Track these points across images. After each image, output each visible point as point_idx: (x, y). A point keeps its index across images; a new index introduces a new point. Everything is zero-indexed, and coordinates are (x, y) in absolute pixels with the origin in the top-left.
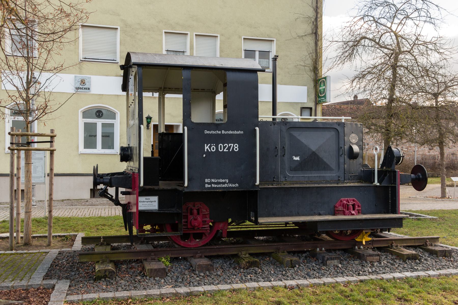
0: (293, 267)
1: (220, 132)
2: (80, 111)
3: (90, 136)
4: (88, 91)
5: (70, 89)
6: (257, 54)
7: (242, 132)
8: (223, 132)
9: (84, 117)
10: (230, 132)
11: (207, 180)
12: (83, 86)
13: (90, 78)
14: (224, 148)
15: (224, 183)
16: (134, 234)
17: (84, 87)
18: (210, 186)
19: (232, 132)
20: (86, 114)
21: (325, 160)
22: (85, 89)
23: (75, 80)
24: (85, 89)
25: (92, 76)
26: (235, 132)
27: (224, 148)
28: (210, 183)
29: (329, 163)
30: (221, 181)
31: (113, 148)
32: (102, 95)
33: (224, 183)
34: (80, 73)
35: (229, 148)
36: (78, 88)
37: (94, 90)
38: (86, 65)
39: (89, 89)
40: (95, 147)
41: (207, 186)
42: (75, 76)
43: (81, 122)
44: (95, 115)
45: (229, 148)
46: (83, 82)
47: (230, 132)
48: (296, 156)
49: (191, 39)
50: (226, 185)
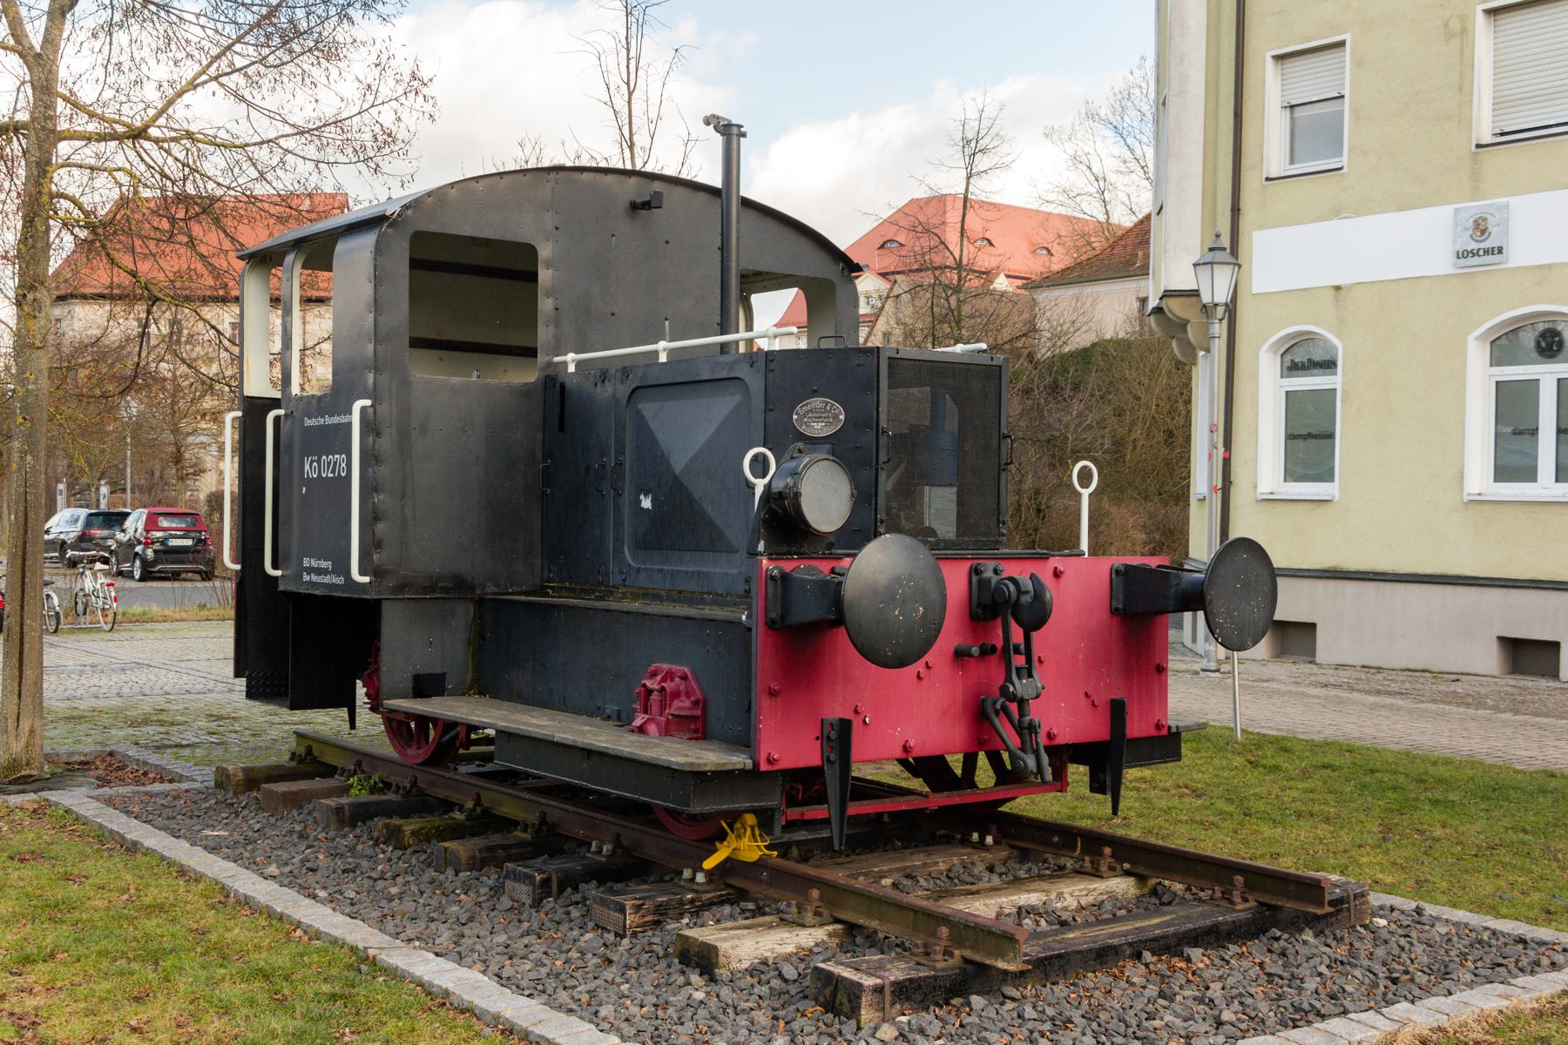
1: (322, 421)
3: (1517, 433)
4: (1496, 258)
5: (1442, 263)
9: (1496, 361)
11: (306, 562)
12: (1481, 245)
13: (1507, 206)
15: (319, 571)
16: (1083, 769)
17: (1483, 245)
19: (322, 421)
20: (1503, 346)
21: (709, 509)
22: (1486, 252)
23: (1456, 226)
24: (1486, 252)
25: (1511, 200)
29: (719, 523)
32: (1550, 266)
34: (1475, 195)
36: (1462, 255)
37: (1521, 253)
38: (1497, 161)
39: (1500, 250)
40: (1529, 474)
41: (306, 578)
42: (1456, 210)
43: (1480, 380)
44: (1534, 355)
46: (1480, 228)
50: (326, 579)
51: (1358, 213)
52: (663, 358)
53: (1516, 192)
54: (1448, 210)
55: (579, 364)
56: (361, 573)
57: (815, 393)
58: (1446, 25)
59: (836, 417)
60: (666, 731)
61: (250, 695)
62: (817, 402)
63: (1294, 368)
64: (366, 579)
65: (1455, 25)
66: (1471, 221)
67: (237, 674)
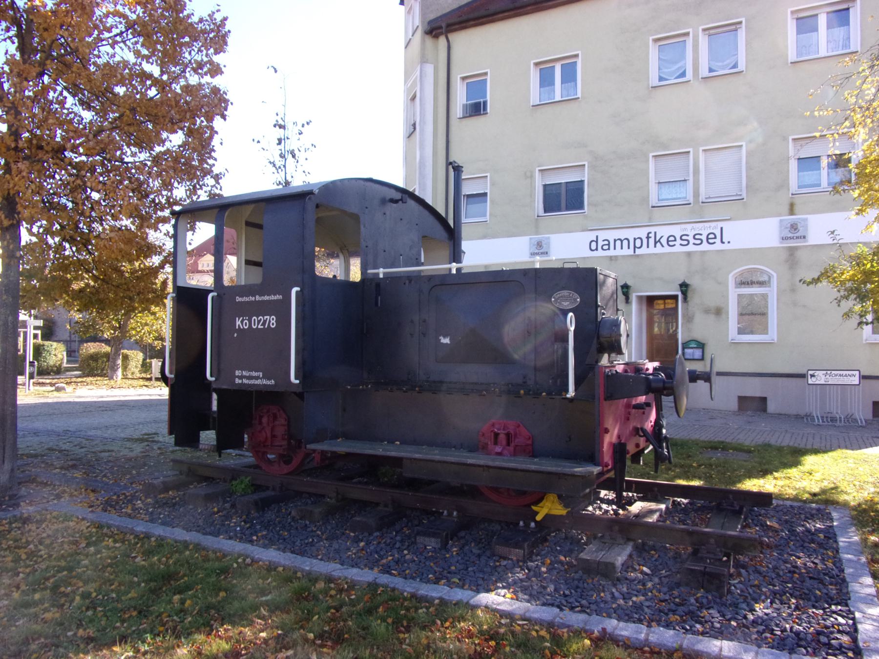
0: (342, 565)
1: (253, 299)
2: (775, 275)
4: (802, 240)
6: (824, 162)
7: (280, 297)
8: (258, 298)
10: (266, 298)
11: (238, 373)
14: (259, 322)
15: (257, 378)
18: (240, 381)
19: (253, 299)
22: (797, 238)
23: (781, 227)
24: (797, 238)
26: (273, 298)
27: (259, 322)
28: (241, 377)
30: (254, 374)
31: (767, 334)
33: (257, 378)
34: (537, 233)
35: (265, 321)
39: (804, 237)
41: (238, 381)
42: (781, 221)
45: (265, 321)
47: (266, 298)
48: (445, 337)
49: (694, 159)
51: (494, 237)
52: (381, 276)
53: (810, 214)
54: (528, 238)
55: (384, 274)
56: (296, 379)
57: (564, 288)
58: (525, 173)
59: (575, 300)
60: (515, 454)
61: (177, 443)
62: (565, 293)
63: (743, 283)
64: (298, 382)
65: (528, 174)
66: (789, 225)
67: (171, 433)
